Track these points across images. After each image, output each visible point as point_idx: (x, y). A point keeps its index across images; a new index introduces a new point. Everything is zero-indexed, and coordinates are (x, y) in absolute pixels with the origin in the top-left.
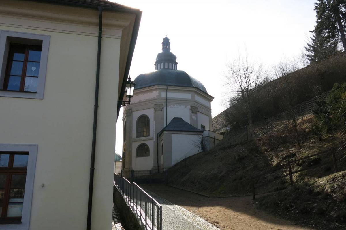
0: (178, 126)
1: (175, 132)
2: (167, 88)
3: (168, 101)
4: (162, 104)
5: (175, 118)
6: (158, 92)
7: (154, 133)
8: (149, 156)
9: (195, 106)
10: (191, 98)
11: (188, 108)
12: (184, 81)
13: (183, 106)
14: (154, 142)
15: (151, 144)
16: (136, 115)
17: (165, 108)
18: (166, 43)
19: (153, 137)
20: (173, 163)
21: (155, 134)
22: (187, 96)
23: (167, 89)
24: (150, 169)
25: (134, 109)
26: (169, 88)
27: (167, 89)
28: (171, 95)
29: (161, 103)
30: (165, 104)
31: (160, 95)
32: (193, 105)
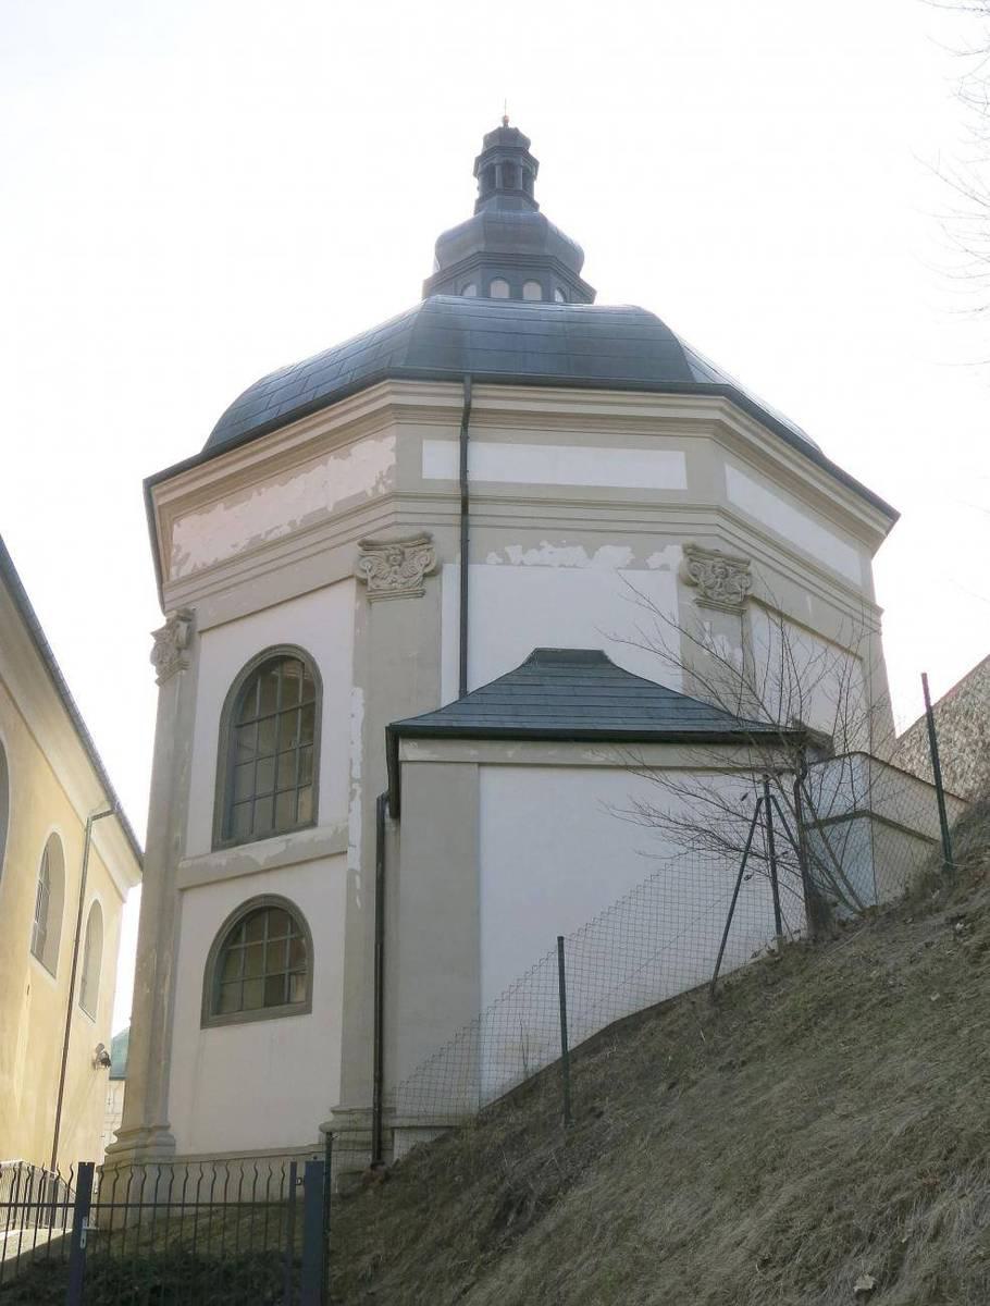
0: (568, 709)
1: (512, 751)
2: (468, 398)
3: (472, 508)
4: (426, 540)
5: (541, 657)
6: (391, 441)
7: (352, 794)
8: (310, 1012)
9: (727, 550)
10: (683, 486)
11: (665, 567)
12: (638, 369)
13: (615, 554)
14: (352, 872)
15: (327, 901)
16: (224, 659)
17: (451, 573)
18: (506, 164)
19: (342, 835)
20: (497, 1075)
21: (357, 805)
22: (654, 468)
23: (467, 415)
24: (303, 1132)
25: (205, 615)
26: (490, 399)
27: (467, 415)
28: (501, 462)
29: (415, 531)
30: (456, 533)
31: (409, 458)
32: (708, 544)
